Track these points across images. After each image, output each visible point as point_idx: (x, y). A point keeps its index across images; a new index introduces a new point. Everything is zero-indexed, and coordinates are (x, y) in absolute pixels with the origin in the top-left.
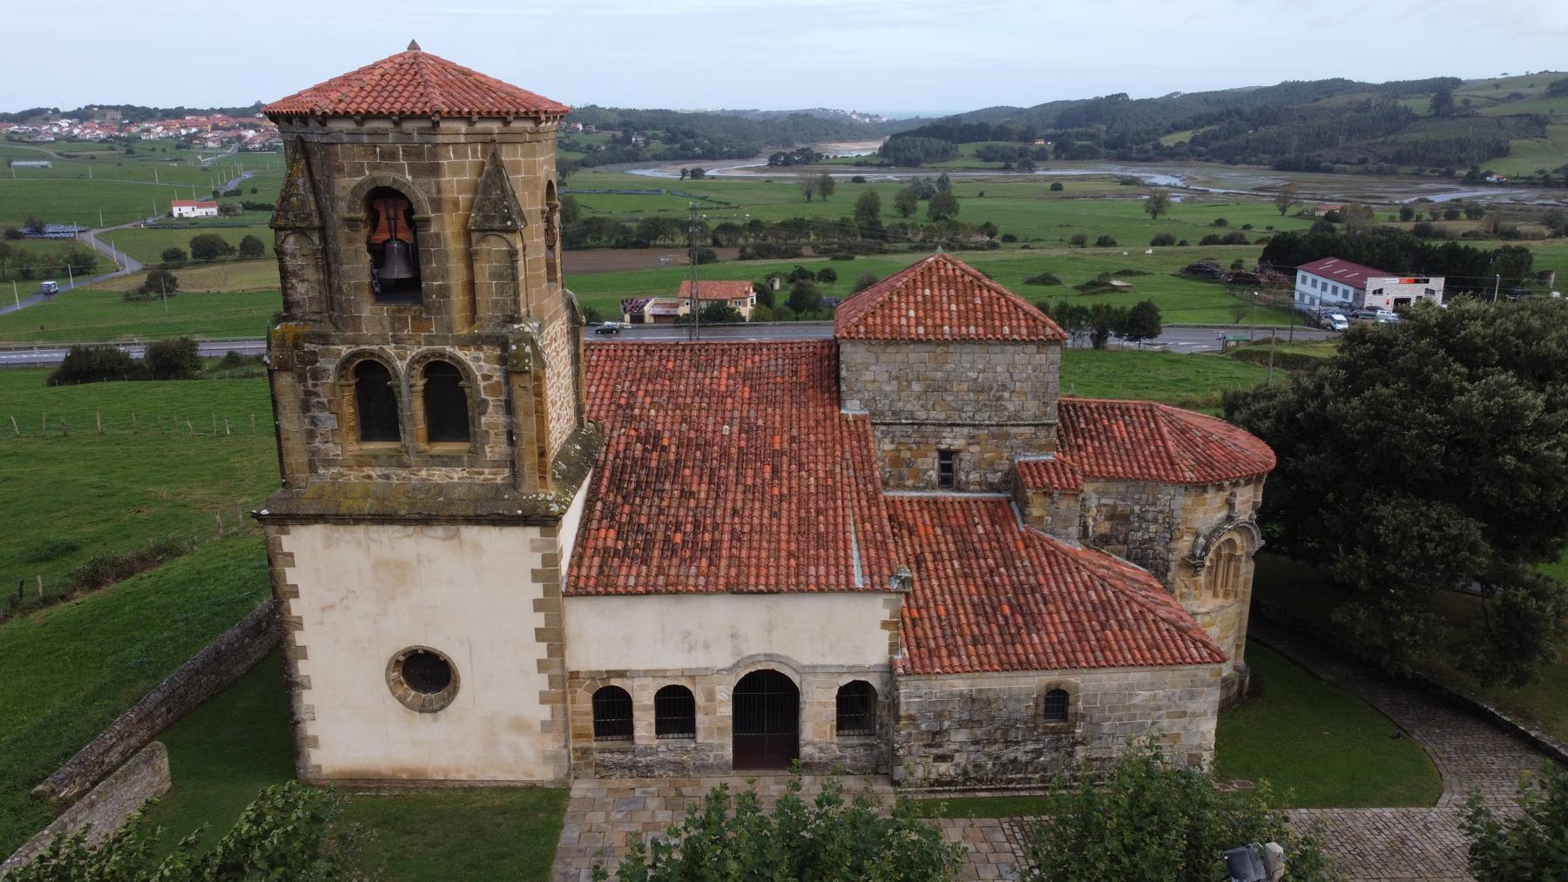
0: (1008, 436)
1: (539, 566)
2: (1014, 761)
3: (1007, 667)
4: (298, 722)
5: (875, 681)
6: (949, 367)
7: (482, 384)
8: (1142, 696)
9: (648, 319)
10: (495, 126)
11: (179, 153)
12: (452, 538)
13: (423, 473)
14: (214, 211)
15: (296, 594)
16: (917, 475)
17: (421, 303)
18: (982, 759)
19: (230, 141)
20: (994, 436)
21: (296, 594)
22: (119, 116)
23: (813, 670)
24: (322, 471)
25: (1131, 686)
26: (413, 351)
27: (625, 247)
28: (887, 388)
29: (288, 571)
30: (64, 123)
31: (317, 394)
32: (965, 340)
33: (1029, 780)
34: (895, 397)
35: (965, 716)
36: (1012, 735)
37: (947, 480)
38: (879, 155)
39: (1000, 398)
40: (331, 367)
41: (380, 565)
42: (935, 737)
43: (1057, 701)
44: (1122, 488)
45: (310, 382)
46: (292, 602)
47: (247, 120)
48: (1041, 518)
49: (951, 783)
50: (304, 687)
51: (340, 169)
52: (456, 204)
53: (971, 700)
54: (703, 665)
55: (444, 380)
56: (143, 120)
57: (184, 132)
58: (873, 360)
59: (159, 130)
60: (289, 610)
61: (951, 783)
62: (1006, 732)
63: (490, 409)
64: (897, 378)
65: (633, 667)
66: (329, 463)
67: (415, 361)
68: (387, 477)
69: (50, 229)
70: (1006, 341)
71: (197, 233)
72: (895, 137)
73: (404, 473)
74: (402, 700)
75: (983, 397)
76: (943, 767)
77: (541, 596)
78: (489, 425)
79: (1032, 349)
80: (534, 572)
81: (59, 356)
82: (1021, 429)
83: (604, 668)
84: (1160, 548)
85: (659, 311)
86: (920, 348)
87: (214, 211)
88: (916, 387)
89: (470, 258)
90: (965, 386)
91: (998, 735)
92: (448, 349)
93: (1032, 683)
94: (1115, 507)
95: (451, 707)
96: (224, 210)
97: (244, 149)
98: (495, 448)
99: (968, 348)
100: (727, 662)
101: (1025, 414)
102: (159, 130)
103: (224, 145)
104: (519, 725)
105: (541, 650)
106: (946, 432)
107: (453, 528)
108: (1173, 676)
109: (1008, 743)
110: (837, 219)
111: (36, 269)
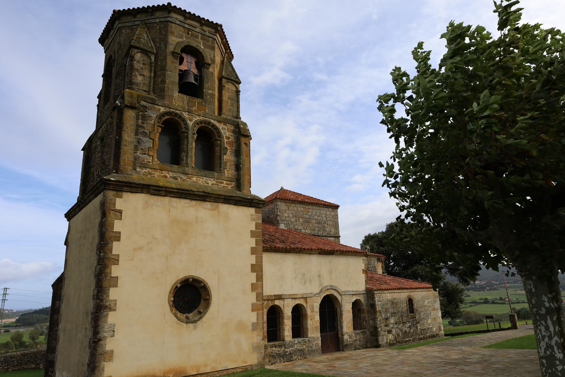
1: (254, 229)
4: (100, 340)
5: (362, 298)
7: (226, 140)
12: (214, 209)
13: (194, 179)
15: (118, 239)
17: (202, 98)
21: (118, 239)
23: (346, 293)
24: (138, 170)
26: (197, 118)
28: (292, 220)
29: (116, 222)
31: (143, 128)
34: (295, 223)
38: (15, 322)
39: (324, 227)
40: (154, 116)
45: (140, 121)
46: (115, 244)
50: (111, 309)
51: (173, 33)
54: (309, 292)
55: (207, 135)
58: (287, 209)
60: (111, 251)
63: (228, 152)
64: (295, 216)
65: (285, 293)
66: (143, 166)
67: (197, 123)
68: (176, 178)
72: (22, 315)
73: (184, 177)
75: (320, 225)
77: (254, 246)
78: (227, 159)
80: (251, 231)
83: (273, 294)
88: (301, 220)
92: (212, 121)
95: (205, 319)
98: (229, 172)
100: (317, 291)
104: (240, 327)
105: (253, 278)
107: (216, 204)
110: (6, 342)
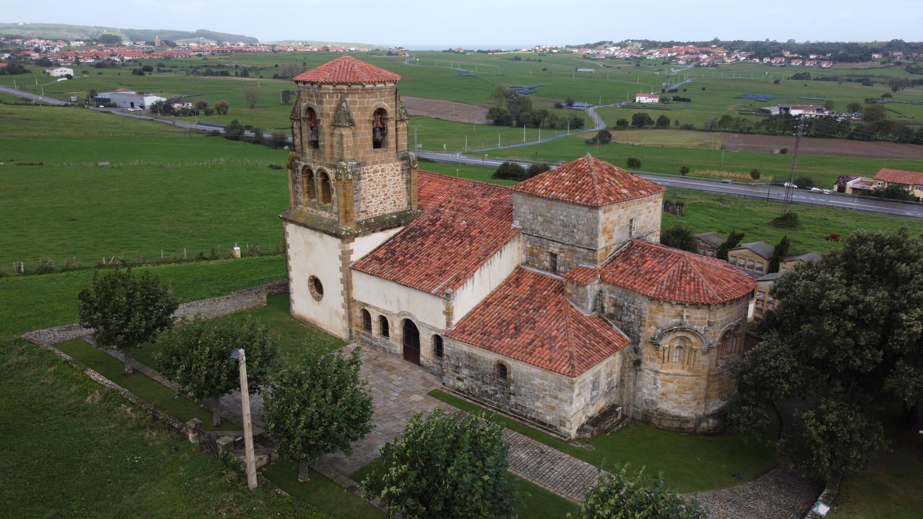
0: (575, 252)
2: (486, 392)
3: (483, 346)
6: (553, 211)
8: (537, 381)
9: (848, 191)
10: (345, 87)
11: (663, 67)
14: (656, 100)
16: (540, 262)
18: (474, 386)
19: (692, 61)
20: (570, 250)
22: (640, 45)
25: (532, 374)
27: (905, 142)
30: (613, 49)
32: (557, 199)
33: (492, 404)
35: (467, 363)
36: (485, 379)
37: (554, 270)
41: (306, 242)
42: (457, 368)
43: (502, 369)
44: (620, 291)
47: (704, 49)
48: (571, 294)
49: (463, 392)
52: (328, 115)
53: (469, 356)
56: (651, 48)
57: (669, 55)
59: (656, 54)
61: (463, 392)
62: (483, 377)
69: (576, 104)
70: (574, 203)
71: (636, 111)
74: (312, 294)
75: (566, 230)
76: (460, 384)
79: (586, 209)
81: (499, 163)
82: (582, 250)
84: (636, 329)
85: (858, 186)
86: (541, 200)
87: (656, 100)
88: (540, 219)
89: (332, 135)
90: (559, 223)
91: (480, 377)
93: (492, 357)
94: (616, 300)
96: (662, 100)
97: (698, 66)
99: (560, 204)
101: (584, 242)
102: (656, 54)
103: (688, 63)
106: (551, 244)
108: (550, 376)
109: (484, 383)
111: (557, 124)
